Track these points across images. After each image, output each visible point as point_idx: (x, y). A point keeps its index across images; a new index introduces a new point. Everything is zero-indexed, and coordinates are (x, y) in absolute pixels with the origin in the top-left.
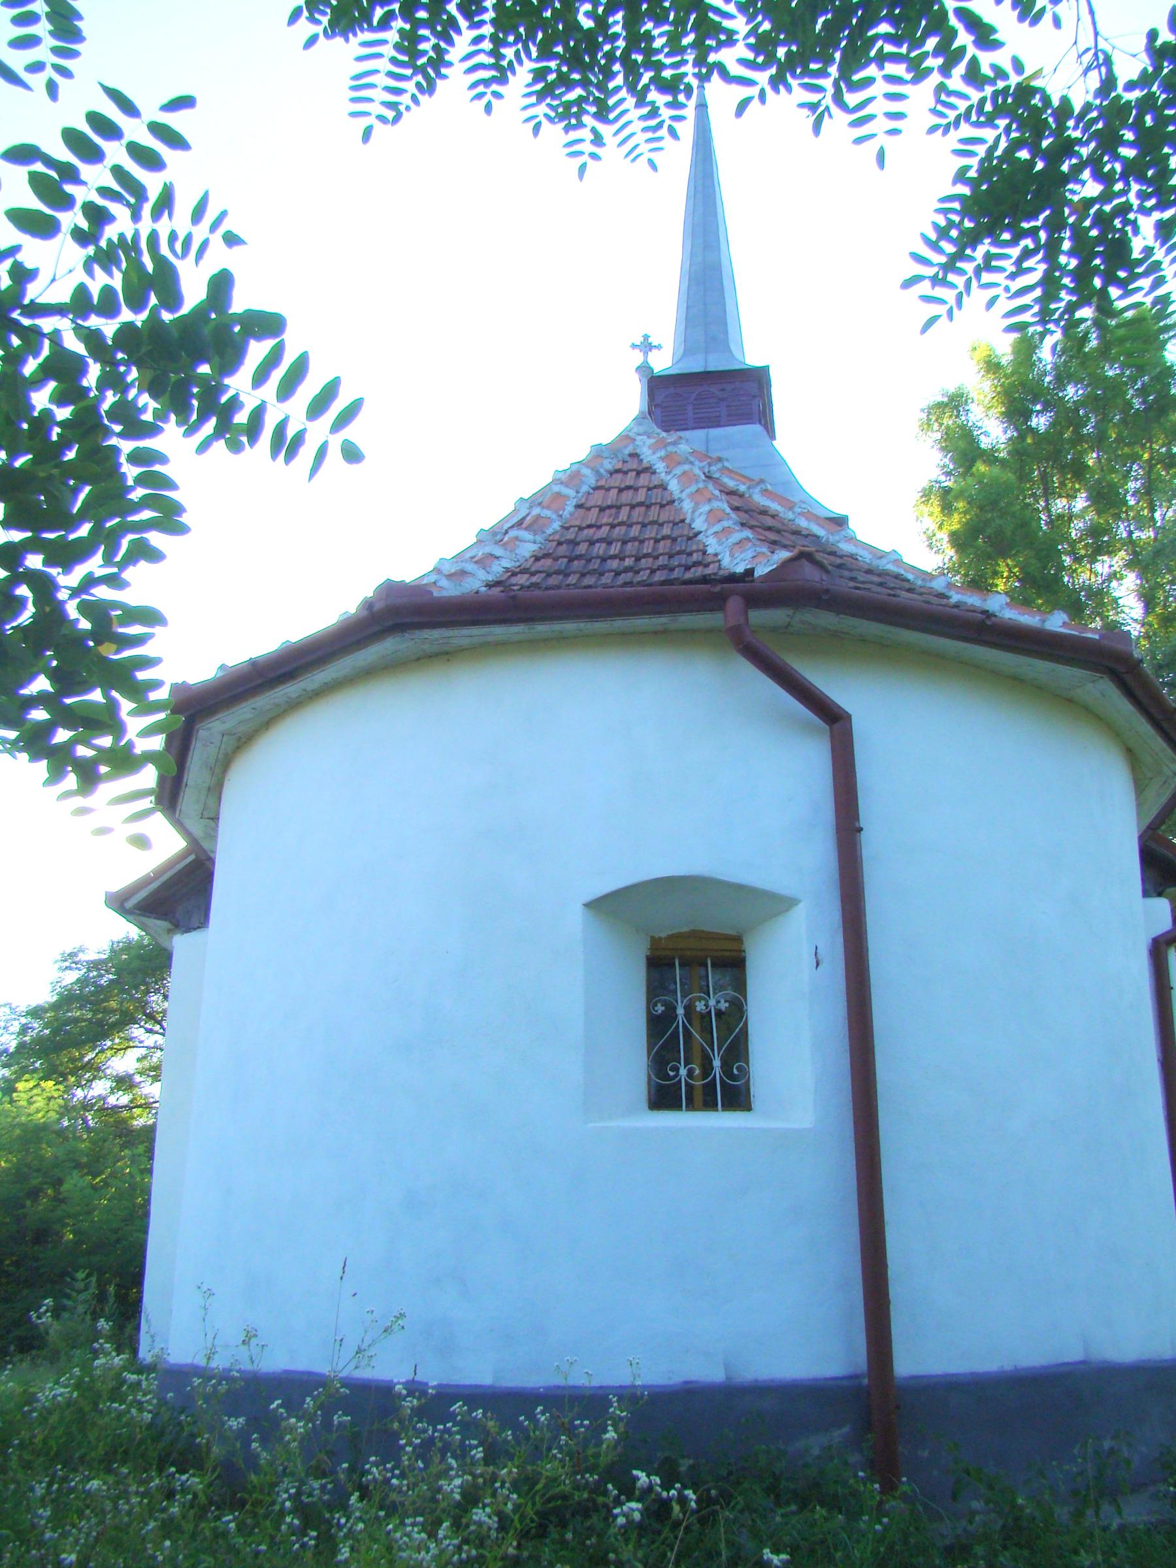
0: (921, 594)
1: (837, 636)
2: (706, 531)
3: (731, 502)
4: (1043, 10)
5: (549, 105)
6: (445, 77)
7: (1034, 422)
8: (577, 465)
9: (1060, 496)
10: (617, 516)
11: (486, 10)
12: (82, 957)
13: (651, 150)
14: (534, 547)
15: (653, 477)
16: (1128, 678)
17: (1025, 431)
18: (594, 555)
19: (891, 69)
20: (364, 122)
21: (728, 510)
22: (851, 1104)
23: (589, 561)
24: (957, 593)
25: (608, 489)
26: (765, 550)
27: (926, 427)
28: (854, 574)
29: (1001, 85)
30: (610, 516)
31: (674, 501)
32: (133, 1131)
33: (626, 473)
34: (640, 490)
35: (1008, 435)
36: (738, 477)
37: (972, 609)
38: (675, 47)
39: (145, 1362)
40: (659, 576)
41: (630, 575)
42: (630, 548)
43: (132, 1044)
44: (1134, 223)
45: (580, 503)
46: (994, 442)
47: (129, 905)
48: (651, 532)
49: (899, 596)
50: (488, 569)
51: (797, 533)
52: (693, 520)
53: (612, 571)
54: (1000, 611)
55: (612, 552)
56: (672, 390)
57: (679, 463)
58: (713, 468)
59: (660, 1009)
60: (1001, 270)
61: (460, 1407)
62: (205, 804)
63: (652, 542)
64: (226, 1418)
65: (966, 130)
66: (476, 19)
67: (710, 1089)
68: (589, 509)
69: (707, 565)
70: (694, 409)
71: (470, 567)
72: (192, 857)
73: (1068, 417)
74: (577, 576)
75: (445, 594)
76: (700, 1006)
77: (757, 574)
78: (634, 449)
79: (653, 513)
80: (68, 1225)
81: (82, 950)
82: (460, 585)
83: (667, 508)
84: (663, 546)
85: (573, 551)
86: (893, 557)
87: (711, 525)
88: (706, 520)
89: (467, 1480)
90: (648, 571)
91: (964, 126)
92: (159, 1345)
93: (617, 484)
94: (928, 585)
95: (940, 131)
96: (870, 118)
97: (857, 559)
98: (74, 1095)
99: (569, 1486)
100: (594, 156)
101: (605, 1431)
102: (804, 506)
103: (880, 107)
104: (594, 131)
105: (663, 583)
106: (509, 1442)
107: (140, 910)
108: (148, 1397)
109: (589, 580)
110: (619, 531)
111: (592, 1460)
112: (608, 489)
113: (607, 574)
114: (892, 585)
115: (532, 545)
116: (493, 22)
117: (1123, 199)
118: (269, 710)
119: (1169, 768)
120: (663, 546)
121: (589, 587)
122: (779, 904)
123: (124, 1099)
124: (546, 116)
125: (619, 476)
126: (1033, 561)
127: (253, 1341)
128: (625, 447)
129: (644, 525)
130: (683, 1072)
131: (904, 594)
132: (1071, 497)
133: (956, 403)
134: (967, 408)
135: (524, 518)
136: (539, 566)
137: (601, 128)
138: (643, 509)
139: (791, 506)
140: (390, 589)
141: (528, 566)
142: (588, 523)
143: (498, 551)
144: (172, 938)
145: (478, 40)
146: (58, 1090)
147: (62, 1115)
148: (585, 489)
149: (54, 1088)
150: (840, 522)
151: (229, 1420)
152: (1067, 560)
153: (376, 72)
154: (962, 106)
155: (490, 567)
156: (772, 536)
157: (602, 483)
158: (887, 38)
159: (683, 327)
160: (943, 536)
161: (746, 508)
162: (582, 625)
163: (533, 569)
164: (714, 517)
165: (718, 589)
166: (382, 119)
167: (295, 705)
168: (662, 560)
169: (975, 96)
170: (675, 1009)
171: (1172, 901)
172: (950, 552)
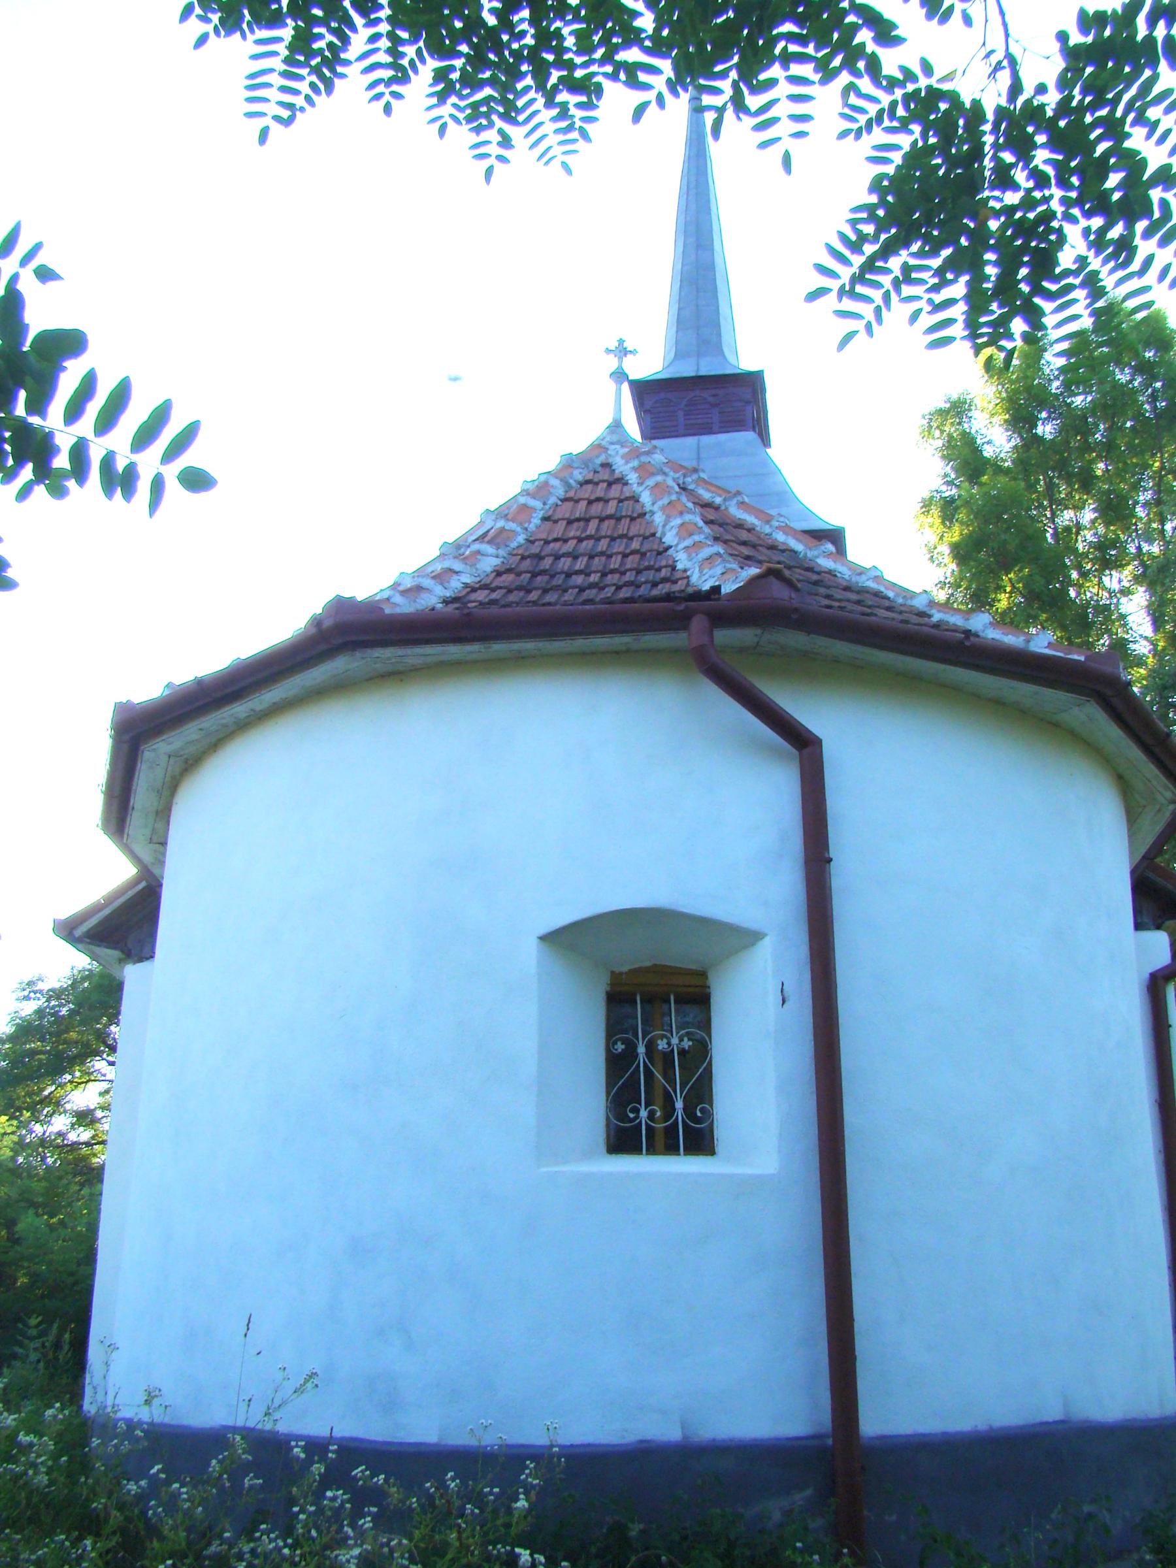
0: (901, 613)
1: (807, 656)
2: (677, 545)
3: (706, 514)
4: (951, 9)
5: (455, 106)
6: (342, 76)
7: (1040, 430)
8: (545, 476)
9: (1067, 508)
10: (585, 530)
11: (381, 7)
12: (41, 986)
13: (565, 153)
14: (497, 561)
15: (625, 488)
16: (1115, 701)
17: (1031, 442)
18: (559, 570)
19: (796, 69)
20: (260, 123)
21: (701, 523)
22: (817, 1149)
23: (552, 576)
24: (939, 611)
25: (577, 501)
26: (735, 566)
27: (926, 433)
28: (830, 592)
29: (910, 87)
30: (577, 530)
31: (645, 514)
32: (93, 1169)
33: (597, 484)
34: (611, 503)
35: (1013, 443)
36: (713, 489)
37: (953, 628)
38: (585, 46)
39: (88, 1415)
40: (625, 593)
41: (594, 591)
42: (597, 562)
43: (93, 1078)
44: (1059, 231)
45: (546, 516)
46: (998, 450)
47: (78, 932)
48: (619, 546)
49: (876, 615)
50: (446, 585)
51: (773, 548)
52: (664, 534)
53: (576, 587)
54: (984, 631)
55: (577, 567)
56: (662, 395)
57: (653, 474)
58: (689, 480)
59: (620, 1047)
60: (921, 282)
61: (362, 1471)
62: (154, 829)
63: (620, 557)
64: (125, 1482)
65: (878, 136)
66: (372, 17)
67: (671, 1131)
68: (556, 522)
69: (675, 582)
70: (685, 415)
71: (427, 583)
72: (143, 884)
73: (1075, 424)
74: (539, 592)
75: (398, 610)
76: (662, 1045)
77: (723, 591)
78: (607, 458)
79: (623, 527)
80: (23, 1267)
81: (40, 979)
82: (415, 601)
83: (638, 520)
84: (631, 562)
85: (537, 565)
86: (873, 574)
87: (682, 538)
88: (677, 534)
89: (366, 1550)
90: (614, 588)
91: (876, 130)
92: (100, 1397)
93: (587, 496)
94: (909, 602)
95: (852, 135)
96: (774, 121)
97: (835, 576)
98: (32, 1132)
99: (476, 1558)
100: (502, 159)
101: (517, 1500)
102: (782, 519)
103: (784, 109)
104: (501, 132)
105: (626, 601)
106: (413, 1510)
107: (88, 938)
108: (43, 1458)
109: (551, 597)
110: (587, 545)
111: (503, 1530)
112: (577, 501)
113: (570, 591)
114: (870, 603)
115: (494, 559)
116: (390, 19)
117: (1044, 207)
118: (217, 731)
119: (1162, 795)
120: (631, 562)
121: (549, 604)
122: (747, 938)
123: (85, 1135)
124: (452, 116)
125: (590, 487)
126: (1037, 578)
127: (156, 1402)
128: (598, 457)
129: (613, 539)
130: (644, 1114)
131: (882, 613)
132: (1078, 507)
133: (958, 409)
134: (969, 415)
135: (488, 531)
136: (499, 581)
137: (509, 129)
138: (613, 522)
139: (768, 520)
140: (340, 605)
141: (488, 582)
142: (555, 536)
143: (457, 566)
144: (123, 968)
145: (375, 38)
146: (12, 1125)
147: (16, 1153)
148: (552, 500)
149: (7, 1123)
150: (834, 537)
151: (128, 1484)
152: (1074, 575)
153: (272, 71)
154: (873, 110)
155: (448, 582)
156: (746, 551)
157: (571, 494)
158: (791, 38)
159: (674, 329)
160: (945, 549)
161: (721, 521)
162: (541, 645)
163: (493, 585)
164: (686, 530)
165: (682, 607)
166: (277, 119)
167: (243, 726)
168: (629, 576)
169: (885, 99)
170: (635, 1047)
171: (1170, 935)
172: (953, 566)
